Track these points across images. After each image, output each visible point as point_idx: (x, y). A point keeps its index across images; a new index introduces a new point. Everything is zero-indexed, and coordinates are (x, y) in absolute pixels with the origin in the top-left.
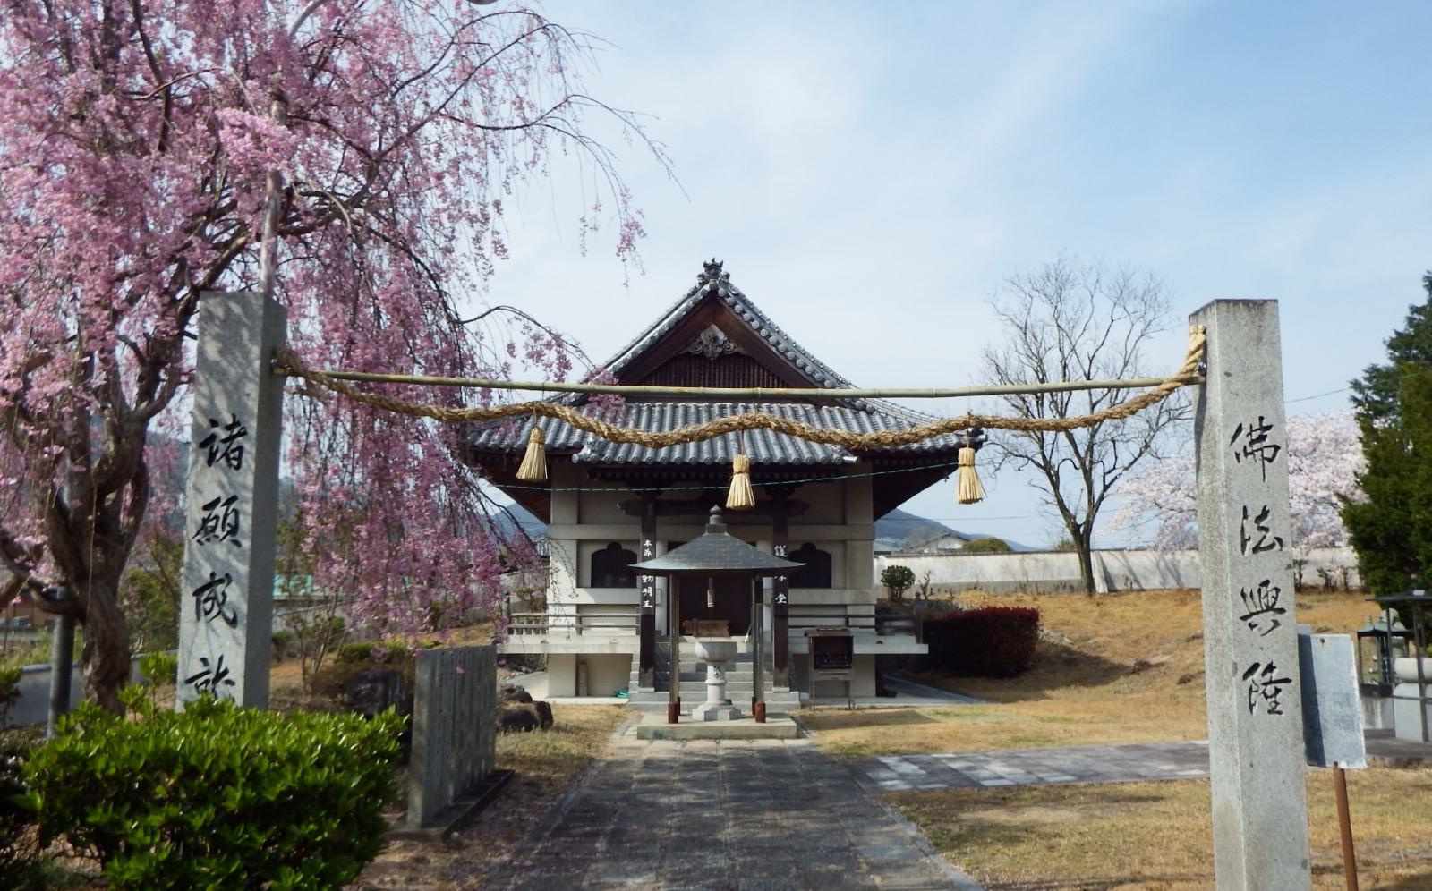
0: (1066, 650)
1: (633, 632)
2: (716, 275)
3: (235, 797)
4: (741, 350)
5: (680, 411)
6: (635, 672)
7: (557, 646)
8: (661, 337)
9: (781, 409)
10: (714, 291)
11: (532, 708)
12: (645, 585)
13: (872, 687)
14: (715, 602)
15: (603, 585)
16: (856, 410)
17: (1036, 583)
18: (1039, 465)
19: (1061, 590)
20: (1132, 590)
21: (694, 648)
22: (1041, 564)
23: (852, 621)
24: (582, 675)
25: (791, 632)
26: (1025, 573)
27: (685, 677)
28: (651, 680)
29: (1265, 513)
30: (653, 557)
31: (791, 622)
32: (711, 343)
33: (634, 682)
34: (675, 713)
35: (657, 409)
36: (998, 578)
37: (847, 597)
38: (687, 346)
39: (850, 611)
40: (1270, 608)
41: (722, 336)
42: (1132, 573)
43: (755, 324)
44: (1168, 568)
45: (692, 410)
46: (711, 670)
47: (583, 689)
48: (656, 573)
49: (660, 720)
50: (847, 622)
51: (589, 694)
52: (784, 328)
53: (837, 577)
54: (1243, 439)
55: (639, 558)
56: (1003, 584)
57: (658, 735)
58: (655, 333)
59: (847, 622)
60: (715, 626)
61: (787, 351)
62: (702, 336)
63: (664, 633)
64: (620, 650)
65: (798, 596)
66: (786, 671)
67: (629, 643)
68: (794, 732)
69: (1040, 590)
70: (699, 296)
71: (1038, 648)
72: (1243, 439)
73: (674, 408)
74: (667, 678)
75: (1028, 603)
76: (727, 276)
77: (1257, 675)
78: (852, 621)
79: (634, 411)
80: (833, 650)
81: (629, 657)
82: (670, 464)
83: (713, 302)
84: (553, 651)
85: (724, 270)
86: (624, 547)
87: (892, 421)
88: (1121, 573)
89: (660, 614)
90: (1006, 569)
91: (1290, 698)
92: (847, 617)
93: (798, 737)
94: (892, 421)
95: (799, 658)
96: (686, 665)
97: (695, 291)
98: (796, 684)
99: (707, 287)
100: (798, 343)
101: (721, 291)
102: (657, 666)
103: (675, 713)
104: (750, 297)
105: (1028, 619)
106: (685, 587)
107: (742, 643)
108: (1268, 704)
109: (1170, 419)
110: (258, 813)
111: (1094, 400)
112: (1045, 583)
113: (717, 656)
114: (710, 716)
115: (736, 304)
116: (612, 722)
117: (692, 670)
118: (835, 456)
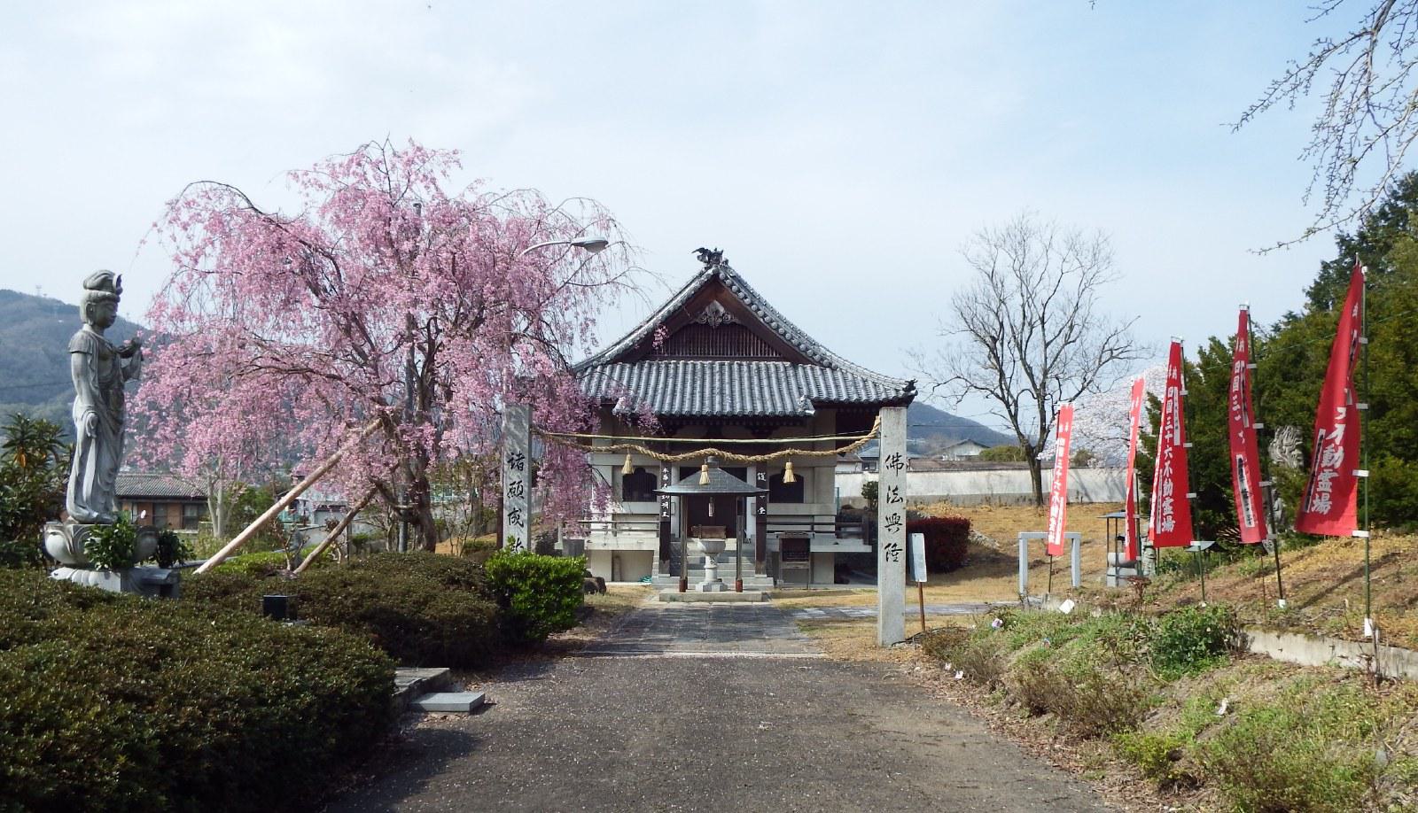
0: (995, 552)
1: (654, 535)
2: (718, 261)
3: (552, 575)
4: (736, 320)
5: (690, 368)
6: (656, 563)
7: (598, 544)
8: (675, 311)
9: (767, 365)
10: (716, 275)
11: (593, 580)
12: (663, 501)
13: (832, 576)
14: (715, 513)
15: (631, 500)
16: (823, 368)
17: (1000, 497)
18: (997, 396)
19: (1021, 503)
20: (1082, 503)
21: (696, 546)
22: (1005, 479)
23: (816, 528)
24: (617, 567)
25: (768, 536)
26: (991, 488)
27: (691, 567)
28: (667, 569)
29: (896, 489)
30: (669, 483)
31: (769, 528)
32: (714, 318)
33: (655, 570)
34: (684, 587)
35: (672, 366)
36: (967, 492)
37: (815, 509)
38: (696, 317)
39: (817, 520)
40: (896, 523)
41: (722, 310)
42: (1083, 488)
43: (747, 301)
44: (1116, 485)
45: (699, 367)
46: (708, 559)
47: (616, 577)
48: (671, 494)
49: (676, 591)
50: (813, 528)
51: (622, 581)
52: (771, 303)
53: (807, 494)
54: (890, 461)
55: (659, 483)
56: (971, 497)
57: (673, 599)
58: (670, 307)
59: (813, 528)
60: (715, 531)
61: (772, 322)
62: (707, 309)
63: (677, 536)
64: (645, 548)
65: (774, 509)
66: (765, 562)
67: (652, 542)
68: (760, 598)
69: (1003, 502)
70: (703, 278)
71: (971, 550)
72: (890, 461)
73: (685, 364)
74: (679, 568)
75: (956, 513)
76: (726, 262)
77: (890, 548)
78: (816, 528)
79: (654, 368)
80: (796, 548)
81: (652, 552)
82: (682, 415)
83: (716, 284)
84: (596, 548)
85: (724, 257)
86: (647, 471)
87: (850, 377)
88: (1074, 488)
89: (674, 521)
90: (974, 484)
91: (902, 556)
92: (813, 524)
93: (762, 601)
94: (850, 377)
95: (774, 554)
96: (692, 558)
97: (701, 274)
98: (772, 572)
99: (710, 272)
100: (782, 313)
101: (722, 275)
102: (672, 559)
103: (684, 587)
104: (744, 278)
105: (962, 527)
106: (693, 505)
107: (731, 544)
108: (894, 558)
109: (1112, 357)
110: (558, 581)
111: (1048, 340)
112: (1008, 496)
113: (712, 550)
114: (706, 589)
115: (733, 284)
116: (642, 594)
117: (698, 562)
118: (800, 410)
